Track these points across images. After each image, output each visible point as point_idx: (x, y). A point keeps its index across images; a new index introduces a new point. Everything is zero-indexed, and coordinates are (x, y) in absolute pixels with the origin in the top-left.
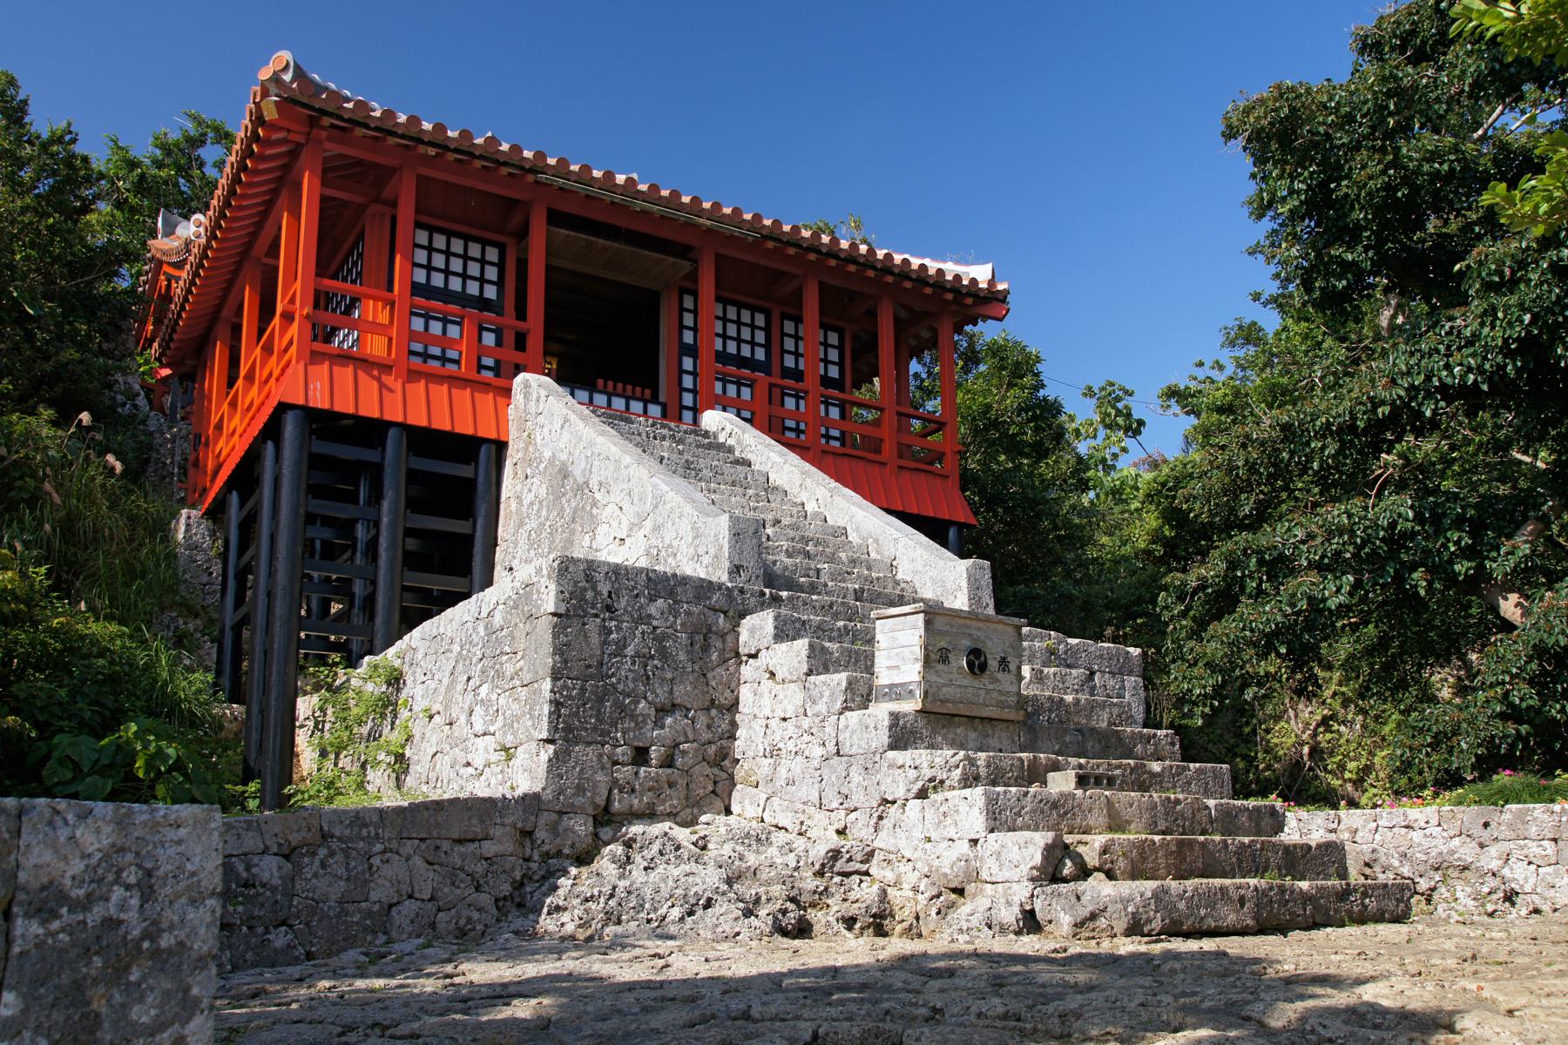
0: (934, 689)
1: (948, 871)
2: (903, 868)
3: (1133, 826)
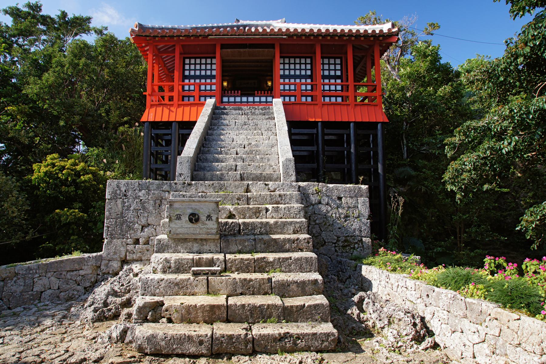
0: (174, 230)
3: (221, 292)
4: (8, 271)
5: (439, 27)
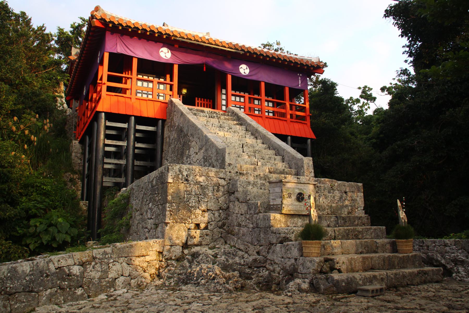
1: (288, 268)
2: (276, 266)
4: (87, 255)
5: (325, 65)
